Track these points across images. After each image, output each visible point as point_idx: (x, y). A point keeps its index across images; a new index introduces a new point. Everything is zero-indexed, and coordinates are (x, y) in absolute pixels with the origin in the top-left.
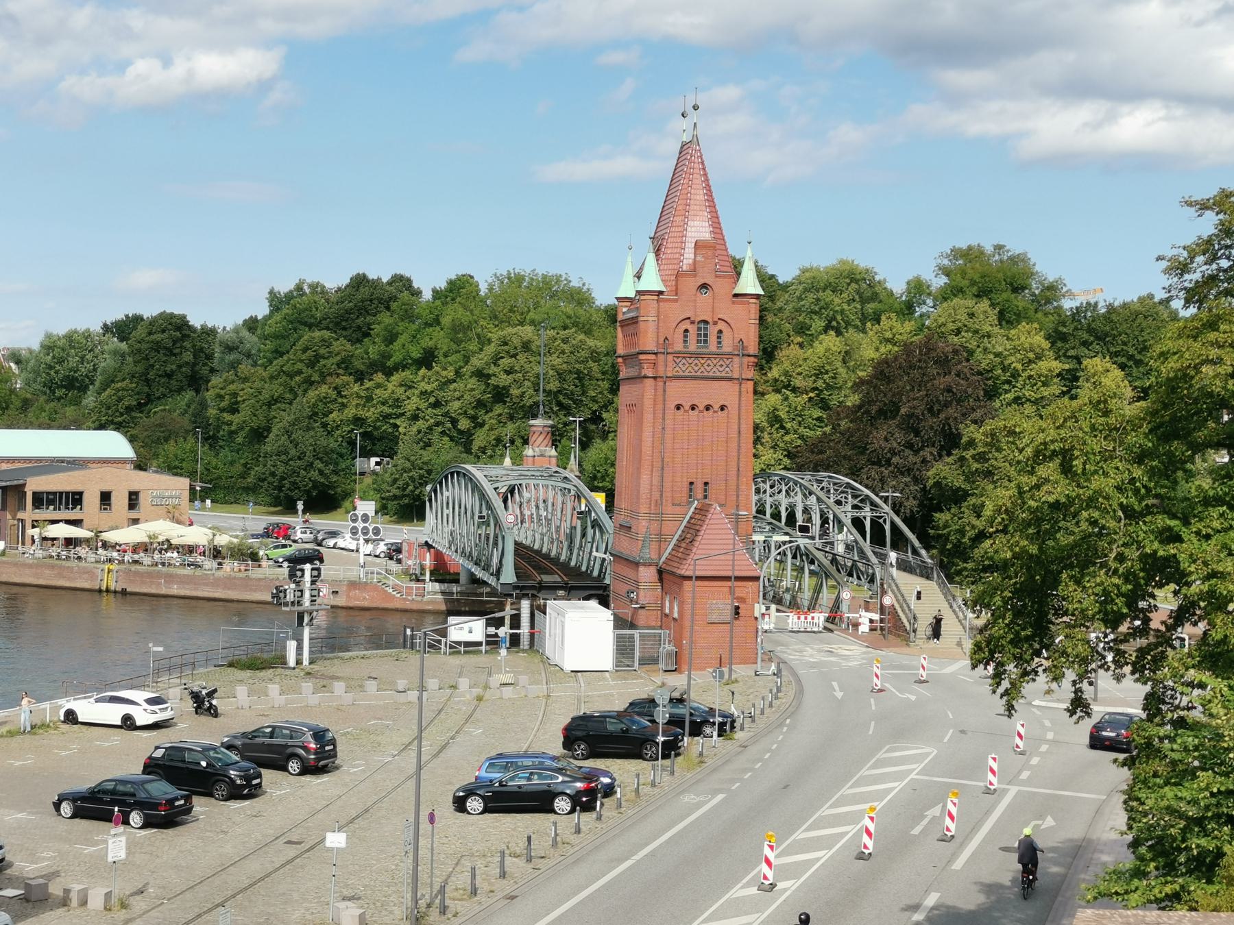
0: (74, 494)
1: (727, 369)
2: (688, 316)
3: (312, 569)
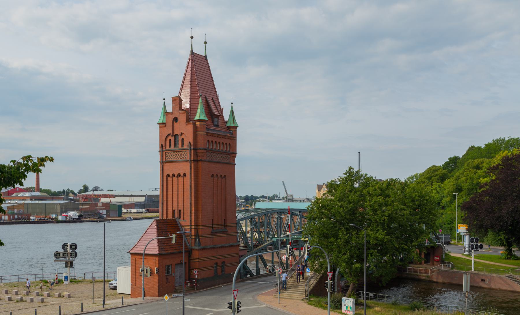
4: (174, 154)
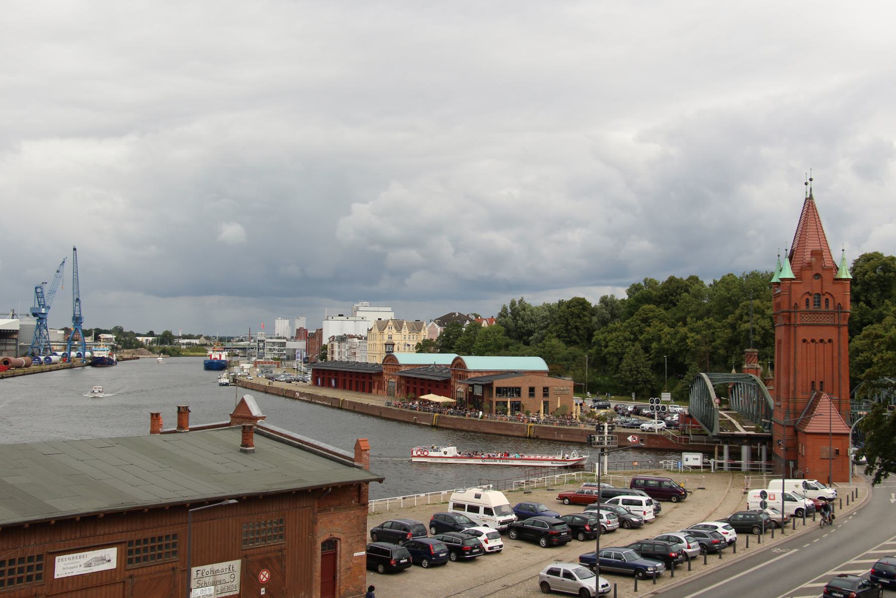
0: (516, 388)
1: (832, 320)
2: (808, 291)
3: (608, 426)
4: (814, 316)
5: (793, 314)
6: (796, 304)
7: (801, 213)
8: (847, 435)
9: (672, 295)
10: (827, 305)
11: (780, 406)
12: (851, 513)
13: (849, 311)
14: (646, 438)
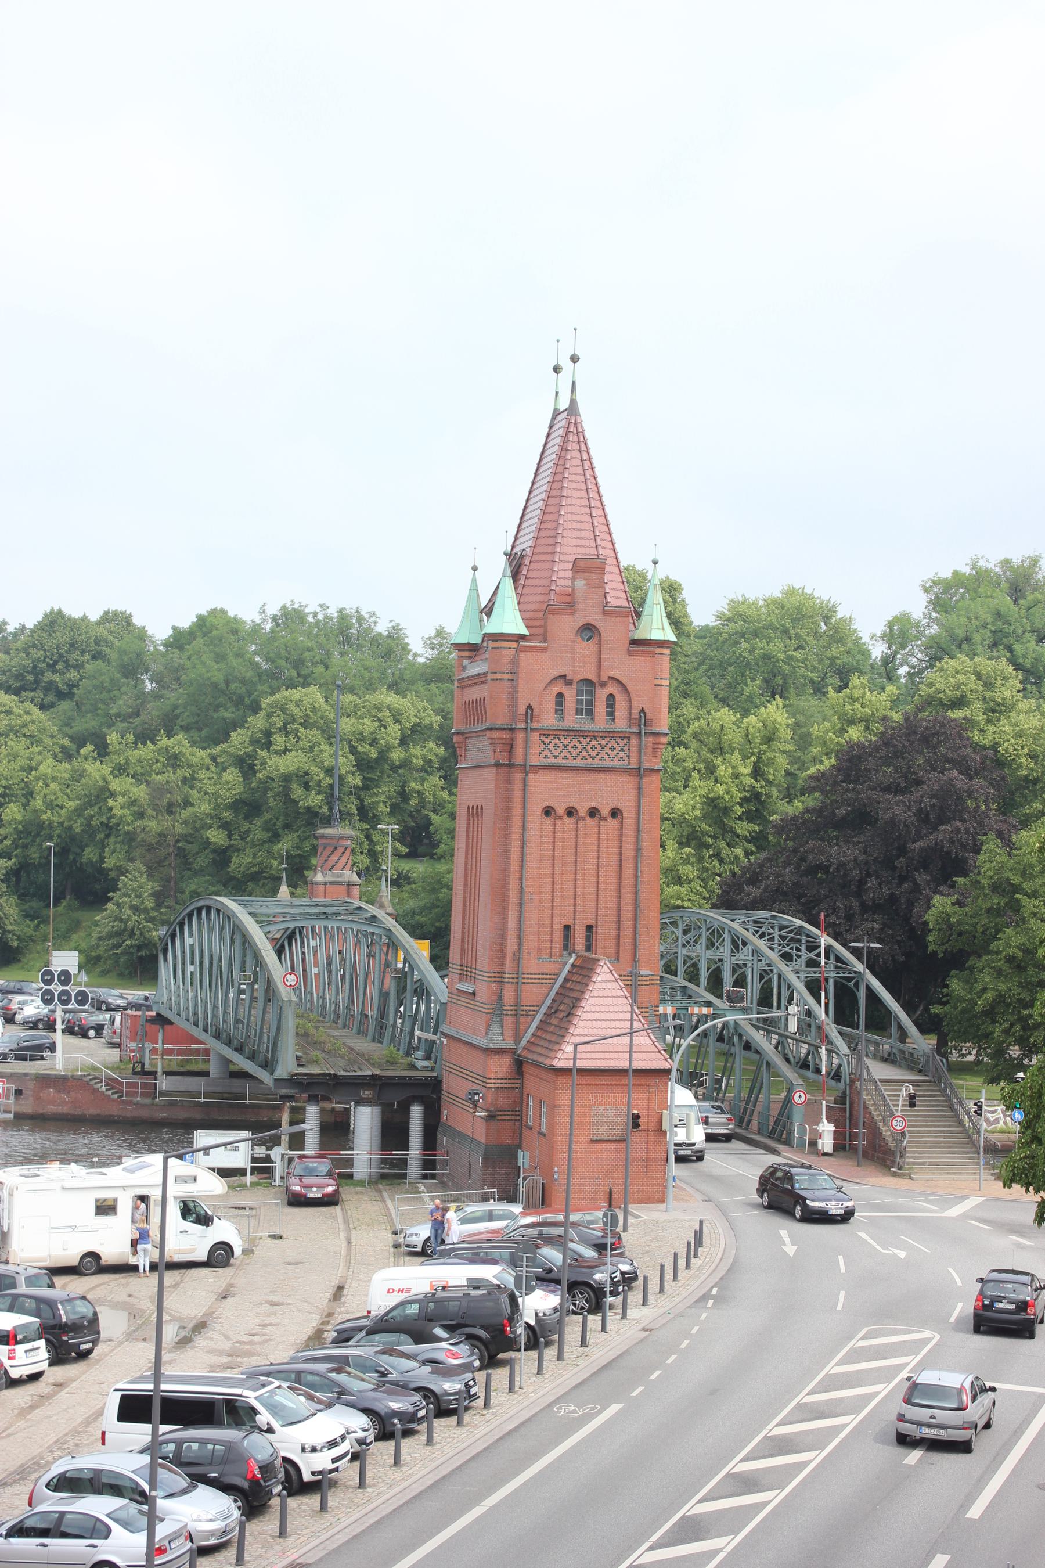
2: (563, 672)
4: (575, 742)
5: (520, 737)
6: (530, 707)
7: (540, 452)
8: (667, 1072)
9: (52, 667)
10: (611, 714)
11: (474, 994)
12: (704, 1291)
13: (665, 729)
14: (31, 1085)
